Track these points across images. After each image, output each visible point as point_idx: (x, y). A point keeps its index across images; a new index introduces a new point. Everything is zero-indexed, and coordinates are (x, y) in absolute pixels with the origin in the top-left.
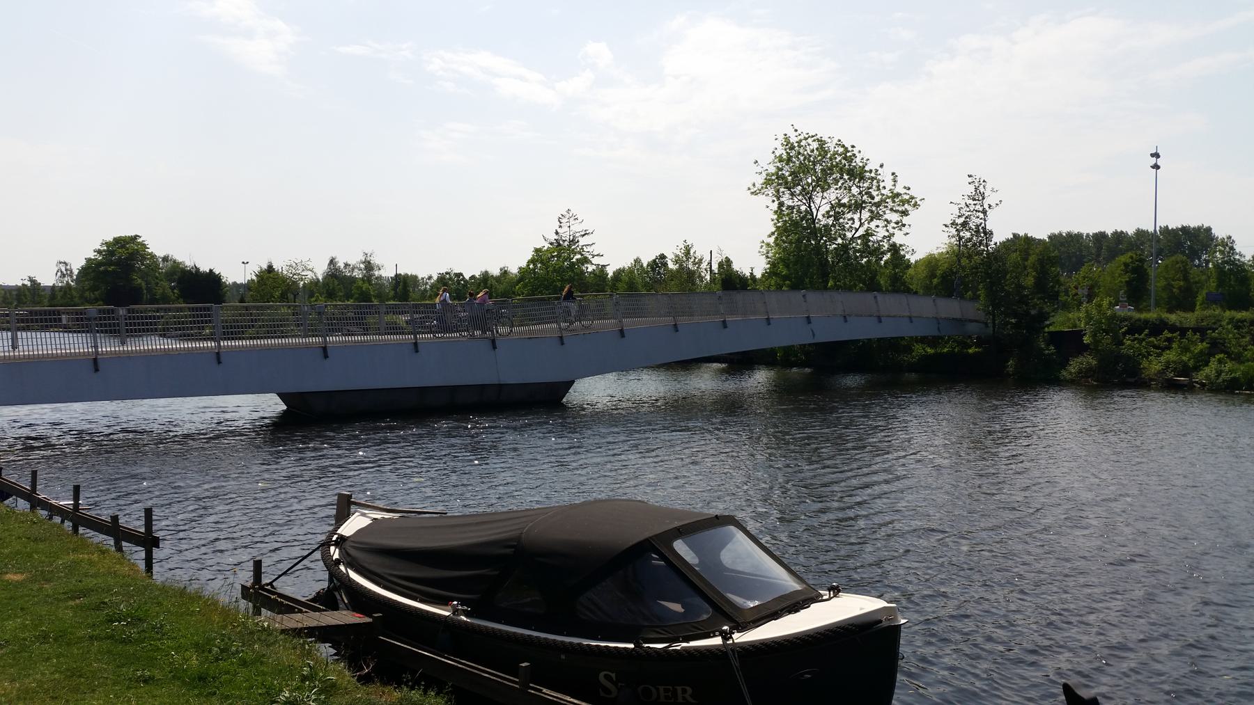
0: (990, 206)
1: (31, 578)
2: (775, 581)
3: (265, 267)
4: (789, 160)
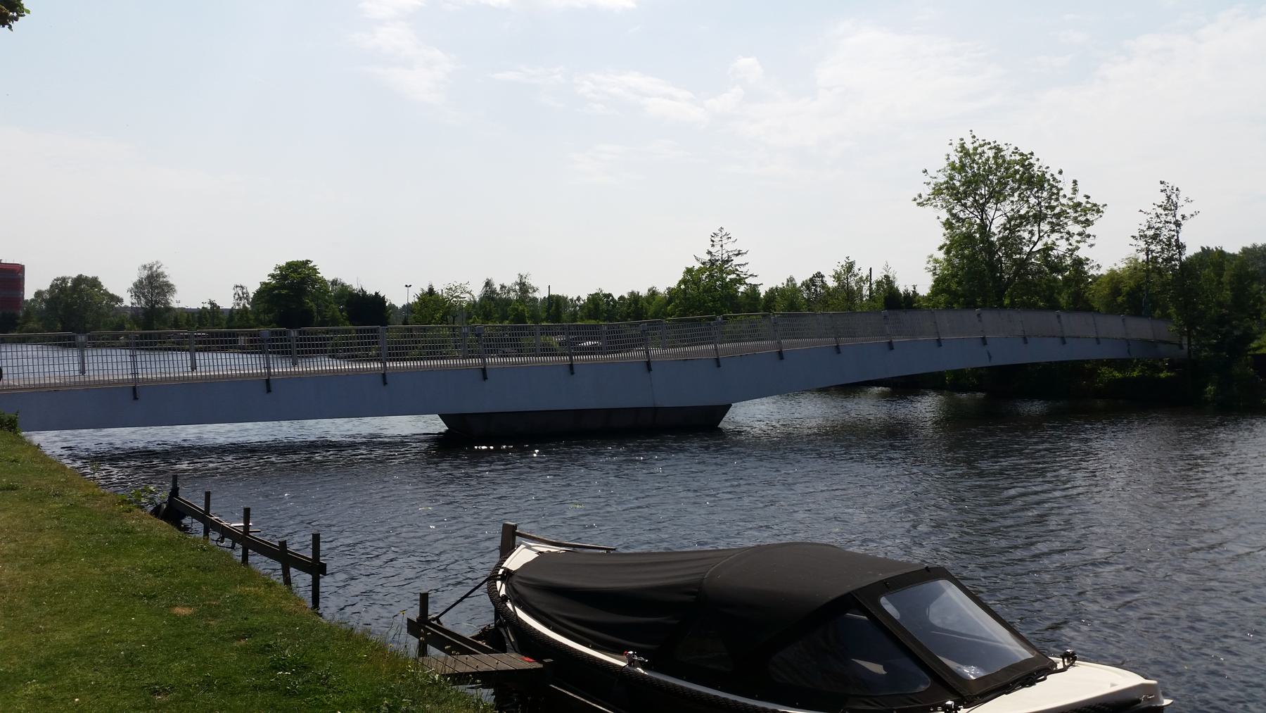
0: (1183, 217)
1: (198, 612)
2: (990, 642)
3: (426, 290)
4: (963, 166)
